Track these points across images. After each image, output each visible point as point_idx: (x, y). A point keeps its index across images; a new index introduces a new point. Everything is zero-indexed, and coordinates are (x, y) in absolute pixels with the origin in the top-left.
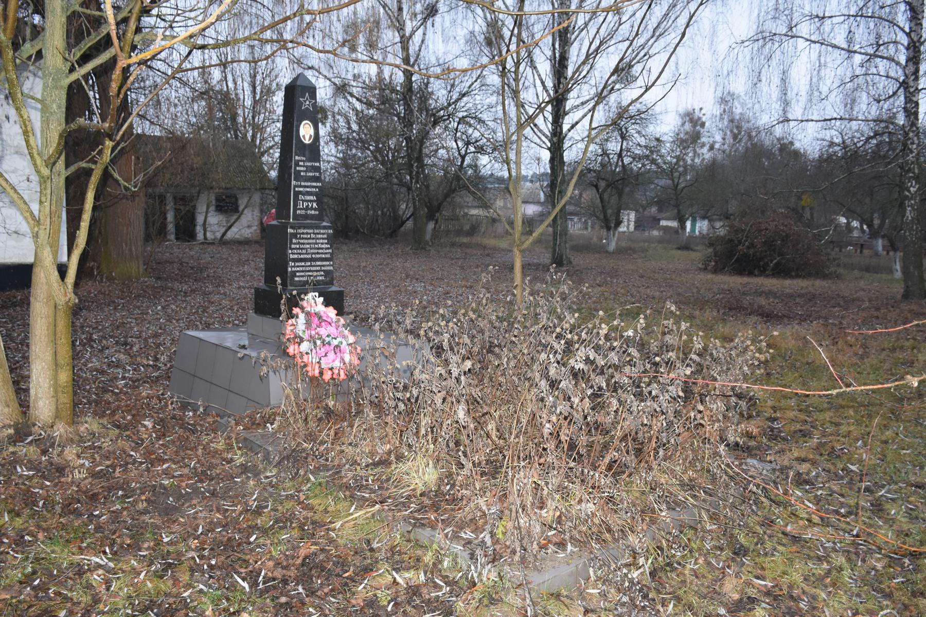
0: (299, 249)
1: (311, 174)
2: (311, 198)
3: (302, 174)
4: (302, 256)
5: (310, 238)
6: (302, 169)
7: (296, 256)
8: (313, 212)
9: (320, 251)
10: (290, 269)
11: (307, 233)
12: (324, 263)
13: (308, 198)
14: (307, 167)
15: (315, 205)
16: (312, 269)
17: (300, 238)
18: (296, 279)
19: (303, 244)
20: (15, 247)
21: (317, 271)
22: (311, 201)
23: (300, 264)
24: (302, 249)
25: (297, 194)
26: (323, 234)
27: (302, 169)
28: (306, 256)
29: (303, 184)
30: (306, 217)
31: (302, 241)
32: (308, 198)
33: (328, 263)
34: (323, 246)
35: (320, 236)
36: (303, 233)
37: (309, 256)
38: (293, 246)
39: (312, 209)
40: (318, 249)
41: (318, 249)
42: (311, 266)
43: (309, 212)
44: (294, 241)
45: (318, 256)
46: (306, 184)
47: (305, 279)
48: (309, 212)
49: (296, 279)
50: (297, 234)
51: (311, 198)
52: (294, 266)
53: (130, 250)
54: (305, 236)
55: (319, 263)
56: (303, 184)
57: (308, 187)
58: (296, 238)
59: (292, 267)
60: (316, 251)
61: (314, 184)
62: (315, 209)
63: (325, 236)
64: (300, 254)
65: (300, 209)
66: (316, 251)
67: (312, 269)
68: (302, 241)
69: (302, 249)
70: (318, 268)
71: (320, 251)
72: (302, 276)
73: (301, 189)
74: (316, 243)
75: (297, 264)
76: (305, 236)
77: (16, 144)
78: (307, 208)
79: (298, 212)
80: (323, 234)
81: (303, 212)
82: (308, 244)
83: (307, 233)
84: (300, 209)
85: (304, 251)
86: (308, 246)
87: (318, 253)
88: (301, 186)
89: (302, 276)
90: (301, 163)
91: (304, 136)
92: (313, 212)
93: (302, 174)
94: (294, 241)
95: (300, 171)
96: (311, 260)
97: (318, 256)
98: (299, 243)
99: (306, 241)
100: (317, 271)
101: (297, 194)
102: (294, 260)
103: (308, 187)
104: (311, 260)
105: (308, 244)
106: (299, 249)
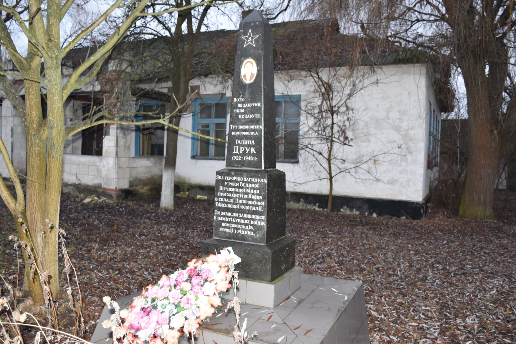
0: (226, 197)
1: (250, 116)
2: (250, 142)
3: (240, 116)
4: (229, 206)
5: (239, 187)
6: (240, 111)
7: (222, 205)
8: (250, 158)
9: (250, 202)
10: (215, 218)
11: (236, 181)
12: (254, 217)
13: (246, 142)
14: (246, 109)
15: (253, 150)
16: (239, 221)
17: (227, 186)
18: (221, 229)
19: (231, 192)
20: (390, 189)
21: (246, 225)
22: (249, 146)
23: (226, 214)
24: (229, 198)
25: (232, 139)
26: (255, 183)
27: (240, 111)
28: (233, 206)
29: (240, 127)
30: (242, 163)
31: (230, 189)
32: (246, 142)
33: (259, 217)
34: (254, 197)
35: (250, 185)
36: (231, 181)
37: (237, 207)
38: (219, 194)
39: (249, 154)
40: (248, 199)
41: (248, 199)
42: (238, 218)
43: (246, 158)
44: (221, 188)
45: (247, 208)
46: (244, 127)
47: (230, 231)
48: (246, 158)
49: (221, 229)
50: (224, 181)
51: (250, 142)
52: (220, 216)
53: (479, 198)
54: (234, 184)
55: (247, 216)
56: (240, 127)
57: (245, 130)
58: (223, 185)
59: (217, 216)
60: (246, 202)
61: (253, 127)
62: (253, 155)
63: (257, 186)
64: (227, 203)
65: (236, 155)
66: (246, 202)
67: (239, 221)
68: (230, 189)
69: (229, 198)
70: (247, 222)
71: (250, 202)
72: (229, 228)
73: (238, 133)
74: (247, 194)
75: (223, 214)
76: (234, 184)
77: (396, 125)
78: (244, 154)
79: (234, 157)
80: (255, 183)
81: (239, 158)
82: (236, 193)
83: (236, 181)
84: (236, 155)
85: (231, 201)
86: (236, 195)
87: (247, 205)
88: (238, 130)
89: (229, 228)
90: (240, 105)
91: (245, 76)
92: (250, 158)
93: (240, 116)
94: (221, 188)
95: (237, 114)
96: (239, 211)
97: (247, 208)
98: (226, 191)
99: (234, 190)
100: (246, 225)
101: (232, 139)
102: (219, 209)
103: (245, 130)
104: (239, 211)
105: (236, 193)
106: (226, 197)
